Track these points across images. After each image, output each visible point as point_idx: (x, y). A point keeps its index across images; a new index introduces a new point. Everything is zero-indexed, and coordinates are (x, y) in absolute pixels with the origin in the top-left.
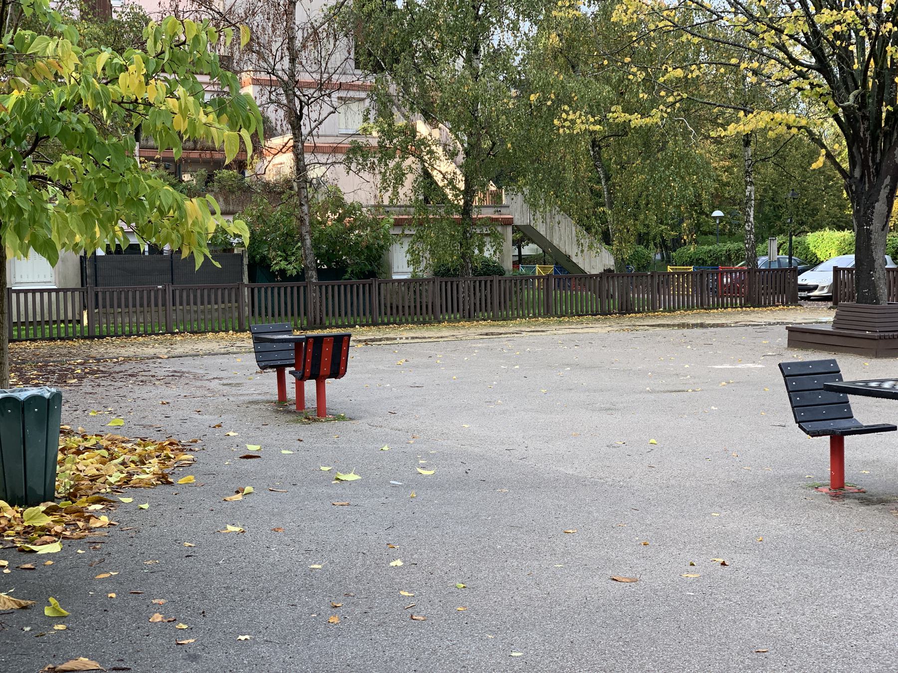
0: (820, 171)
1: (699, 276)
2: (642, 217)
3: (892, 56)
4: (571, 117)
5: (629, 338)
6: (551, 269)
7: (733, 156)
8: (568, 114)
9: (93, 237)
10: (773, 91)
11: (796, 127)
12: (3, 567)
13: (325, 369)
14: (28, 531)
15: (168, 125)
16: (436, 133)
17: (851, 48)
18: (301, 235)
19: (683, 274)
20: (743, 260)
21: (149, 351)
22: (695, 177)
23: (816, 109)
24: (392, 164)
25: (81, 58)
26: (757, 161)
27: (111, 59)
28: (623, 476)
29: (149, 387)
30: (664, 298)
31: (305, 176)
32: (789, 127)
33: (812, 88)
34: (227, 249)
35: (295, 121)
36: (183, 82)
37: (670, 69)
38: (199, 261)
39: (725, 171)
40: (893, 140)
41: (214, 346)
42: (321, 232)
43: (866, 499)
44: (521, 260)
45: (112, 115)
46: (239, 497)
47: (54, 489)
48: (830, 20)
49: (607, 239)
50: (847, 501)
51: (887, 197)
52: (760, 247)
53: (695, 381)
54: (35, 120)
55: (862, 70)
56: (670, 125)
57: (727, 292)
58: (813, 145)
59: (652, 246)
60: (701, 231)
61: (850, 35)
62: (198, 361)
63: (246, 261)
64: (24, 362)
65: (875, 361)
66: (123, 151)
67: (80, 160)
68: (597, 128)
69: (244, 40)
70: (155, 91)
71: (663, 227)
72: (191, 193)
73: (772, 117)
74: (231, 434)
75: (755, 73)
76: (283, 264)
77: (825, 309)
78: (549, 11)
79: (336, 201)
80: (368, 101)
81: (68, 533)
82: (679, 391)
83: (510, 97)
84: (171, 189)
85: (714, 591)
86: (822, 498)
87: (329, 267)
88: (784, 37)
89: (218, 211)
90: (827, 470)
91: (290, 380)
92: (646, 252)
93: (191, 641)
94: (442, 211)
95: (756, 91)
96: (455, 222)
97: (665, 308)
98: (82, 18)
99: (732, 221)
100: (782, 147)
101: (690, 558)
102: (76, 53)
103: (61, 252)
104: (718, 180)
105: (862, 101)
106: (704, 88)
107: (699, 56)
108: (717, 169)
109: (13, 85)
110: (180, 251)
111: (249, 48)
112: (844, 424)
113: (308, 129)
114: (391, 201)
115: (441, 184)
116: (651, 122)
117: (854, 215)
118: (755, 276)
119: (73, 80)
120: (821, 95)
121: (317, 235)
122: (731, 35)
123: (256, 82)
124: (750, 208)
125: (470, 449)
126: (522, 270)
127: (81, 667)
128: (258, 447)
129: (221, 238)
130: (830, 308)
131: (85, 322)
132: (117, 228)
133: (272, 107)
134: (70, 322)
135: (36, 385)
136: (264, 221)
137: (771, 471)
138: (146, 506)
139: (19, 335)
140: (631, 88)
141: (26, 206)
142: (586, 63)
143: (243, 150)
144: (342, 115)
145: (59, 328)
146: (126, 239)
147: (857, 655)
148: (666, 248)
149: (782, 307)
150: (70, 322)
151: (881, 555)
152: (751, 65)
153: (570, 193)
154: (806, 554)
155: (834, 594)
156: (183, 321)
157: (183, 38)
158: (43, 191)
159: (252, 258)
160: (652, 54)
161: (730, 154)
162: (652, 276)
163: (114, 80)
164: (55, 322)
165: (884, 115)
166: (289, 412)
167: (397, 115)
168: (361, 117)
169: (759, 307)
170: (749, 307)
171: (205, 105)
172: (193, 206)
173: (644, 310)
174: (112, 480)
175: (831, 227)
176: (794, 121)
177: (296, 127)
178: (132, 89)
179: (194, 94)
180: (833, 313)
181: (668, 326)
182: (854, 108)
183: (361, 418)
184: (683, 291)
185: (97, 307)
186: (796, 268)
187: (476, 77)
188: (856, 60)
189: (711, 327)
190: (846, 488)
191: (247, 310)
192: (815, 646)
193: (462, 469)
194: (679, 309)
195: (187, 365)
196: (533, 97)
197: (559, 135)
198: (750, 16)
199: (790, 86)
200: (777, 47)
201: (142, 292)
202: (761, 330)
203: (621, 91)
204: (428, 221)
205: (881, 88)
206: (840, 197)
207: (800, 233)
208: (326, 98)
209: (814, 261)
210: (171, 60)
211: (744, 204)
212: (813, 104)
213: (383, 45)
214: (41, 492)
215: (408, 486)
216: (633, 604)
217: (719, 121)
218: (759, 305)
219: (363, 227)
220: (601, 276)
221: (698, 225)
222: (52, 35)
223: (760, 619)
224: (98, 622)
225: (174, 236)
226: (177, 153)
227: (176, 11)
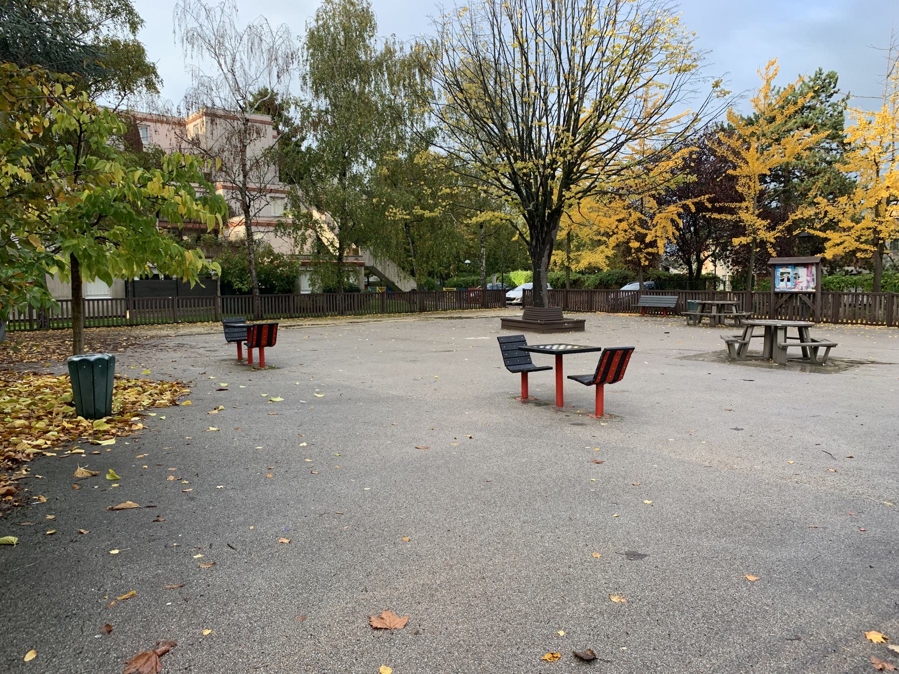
0: (516, 242)
1: (459, 293)
2: (430, 263)
4: (394, 211)
6: (384, 289)
7: (474, 233)
8: (392, 209)
9: (133, 271)
10: (494, 201)
12: (82, 453)
13: (264, 342)
14: (96, 433)
15: (176, 210)
16: (323, 217)
17: (531, 181)
18: (250, 270)
21: (164, 333)
24: (300, 233)
25: (125, 173)
27: (143, 174)
29: (165, 353)
31: (252, 238)
32: (502, 220)
34: (209, 277)
35: (246, 208)
36: (184, 187)
38: (193, 284)
41: (201, 330)
42: (261, 268)
43: (538, 403)
44: (369, 284)
45: (143, 204)
46: (216, 412)
47: (111, 409)
48: (521, 166)
49: (413, 274)
52: (488, 279)
54: (98, 207)
58: (513, 229)
59: (435, 277)
60: (460, 270)
62: (192, 338)
63: (219, 283)
64: (92, 339)
66: (150, 225)
67: (125, 229)
68: (408, 217)
69: (218, 166)
70: (168, 192)
72: (188, 247)
74: (211, 377)
75: (485, 192)
76: (240, 285)
78: (382, 156)
79: (269, 252)
80: (286, 199)
81: (119, 434)
83: (362, 200)
84: (177, 245)
86: (517, 402)
87: (266, 287)
88: (499, 174)
89: (203, 256)
91: (244, 348)
93: (191, 490)
94: (327, 258)
96: (334, 264)
98: (126, 150)
100: (498, 229)
101: (454, 435)
102: (123, 170)
103: (114, 279)
104: (468, 245)
106: (460, 198)
109: (85, 187)
110: (182, 278)
111: (221, 169)
113: (254, 213)
114: (300, 252)
115: (326, 244)
119: (121, 185)
121: (259, 270)
122: (474, 171)
123: (224, 187)
125: (343, 383)
126: (369, 289)
127: (128, 507)
128: (226, 384)
129: (205, 271)
131: (128, 317)
132: (146, 266)
133: (234, 201)
134: (119, 316)
135: (100, 352)
136: (229, 262)
138: (164, 418)
139: (90, 324)
141: (93, 254)
142: (401, 184)
143: (217, 224)
144: (272, 206)
145: (113, 320)
146: (151, 272)
148: (443, 279)
150: (119, 316)
153: (394, 250)
156: (184, 316)
157: (184, 164)
158: (104, 246)
159: (222, 282)
163: (145, 186)
164: (110, 317)
166: (244, 365)
167: (302, 207)
168: (283, 208)
171: (196, 200)
172: (189, 254)
174: (144, 404)
177: (247, 213)
178: (155, 191)
179: (190, 194)
180: (523, 311)
183: (284, 367)
185: (135, 308)
187: (344, 188)
191: (220, 310)
193: (339, 393)
195: (186, 341)
196: (374, 200)
197: (388, 220)
198: (483, 163)
201: (160, 300)
203: (420, 198)
204: (320, 263)
205: (545, 201)
206: (526, 254)
208: (263, 197)
210: (177, 175)
211: (480, 257)
213: (295, 170)
214: (103, 411)
215: (310, 403)
218: (488, 308)
219: (284, 266)
220: (410, 292)
221: (458, 268)
222: (108, 159)
223: (488, 465)
224: (137, 481)
225: (178, 271)
226: (180, 225)
227: (180, 149)
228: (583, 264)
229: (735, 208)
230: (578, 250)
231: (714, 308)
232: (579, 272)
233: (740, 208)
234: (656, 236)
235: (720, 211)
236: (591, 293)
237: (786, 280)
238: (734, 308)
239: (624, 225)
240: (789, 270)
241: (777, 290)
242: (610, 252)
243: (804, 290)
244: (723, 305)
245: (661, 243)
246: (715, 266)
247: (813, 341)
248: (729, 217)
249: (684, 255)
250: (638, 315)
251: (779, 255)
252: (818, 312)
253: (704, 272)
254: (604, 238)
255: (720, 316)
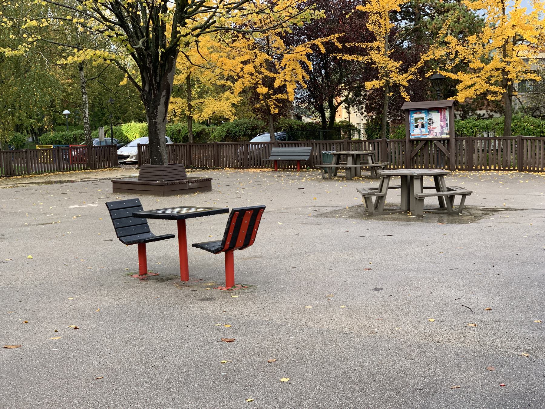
2: (17, 114)
3: (162, 19)
5: (12, 192)
7: (73, 77)
11: (109, 60)
17: (138, 13)
19: (46, 150)
20: (84, 140)
22: (50, 89)
23: (121, 49)
26: (88, 80)
28: (11, 280)
30: (35, 165)
32: (105, 60)
33: (117, 36)
37: (28, 21)
39: (69, 86)
40: (166, 69)
43: (160, 279)
50: (149, 281)
51: (164, 102)
52: (94, 133)
53: (56, 217)
55: (145, 27)
56: (31, 56)
57: (75, 160)
60: (56, 123)
61: (137, 5)
65: (164, 199)
71: (32, 121)
73: (94, 53)
75: (83, 25)
77: (134, 169)
82: (46, 224)
85: (70, 346)
88: (99, 4)
90: (136, 264)
92: (22, 136)
95: (85, 37)
97: (36, 172)
99: (76, 117)
101: (55, 327)
104: (64, 91)
105: (147, 44)
107: (47, 13)
108: (64, 84)
112: (145, 236)
116: (18, 53)
117: (146, 113)
118: (92, 151)
120: (123, 40)
124: (86, 109)
130: (137, 169)
137: (105, 268)
140: (4, 32)
147: (156, 371)
149: (109, 169)
151: (169, 310)
152: (79, 20)
154: (125, 315)
155: (142, 337)
160: (17, 11)
161: (72, 76)
162: (26, 152)
165: (160, 54)
169: (95, 169)
170: (89, 170)
173: (22, 173)
175: (135, 120)
176: (108, 56)
180: (138, 171)
181: (39, 183)
182: (142, 49)
184: (47, 161)
186: (116, 145)
188: (142, 21)
189: (66, 183)
190: (148, 273)
192: (131, 370)
194: (45, 172)
199: (104, 34)
200: (94, 10)
202: (97, 183)
205: (157, 38)
207: (117, 124)
209: (126, 141)
211: (82, 106)
212: (119, 46)
216: (18, 362)
217: (63, 55)
218: (95, 168)
221: (54, 119)
223: (98, 359)
228: (207, 113)
229: (366, 48)
230: (200, 97)
231: (350, 159)
232: (203, 123)
233: (371, 48)
234: (285, 81)
235: (351, 51)
236: (217, 146)
237: (420, 126)
238: (369, 159)
239: (249, 68)
240: (423, 115)
241: (412, 137)
242: (236, 99)
243: (439, 136)
244: (358, 155)
245: (290, 88)
246: (349, 113)
247: (449, 190)
248: (360, 59)
249: (316, 102)
250: (271, 170)
251: (413, 99)
252: (453, 159)
253: (338, 120)
254: (229, 83)
255: (356, 168)
